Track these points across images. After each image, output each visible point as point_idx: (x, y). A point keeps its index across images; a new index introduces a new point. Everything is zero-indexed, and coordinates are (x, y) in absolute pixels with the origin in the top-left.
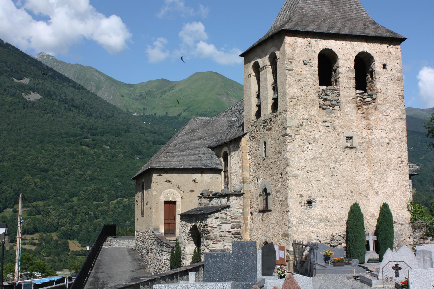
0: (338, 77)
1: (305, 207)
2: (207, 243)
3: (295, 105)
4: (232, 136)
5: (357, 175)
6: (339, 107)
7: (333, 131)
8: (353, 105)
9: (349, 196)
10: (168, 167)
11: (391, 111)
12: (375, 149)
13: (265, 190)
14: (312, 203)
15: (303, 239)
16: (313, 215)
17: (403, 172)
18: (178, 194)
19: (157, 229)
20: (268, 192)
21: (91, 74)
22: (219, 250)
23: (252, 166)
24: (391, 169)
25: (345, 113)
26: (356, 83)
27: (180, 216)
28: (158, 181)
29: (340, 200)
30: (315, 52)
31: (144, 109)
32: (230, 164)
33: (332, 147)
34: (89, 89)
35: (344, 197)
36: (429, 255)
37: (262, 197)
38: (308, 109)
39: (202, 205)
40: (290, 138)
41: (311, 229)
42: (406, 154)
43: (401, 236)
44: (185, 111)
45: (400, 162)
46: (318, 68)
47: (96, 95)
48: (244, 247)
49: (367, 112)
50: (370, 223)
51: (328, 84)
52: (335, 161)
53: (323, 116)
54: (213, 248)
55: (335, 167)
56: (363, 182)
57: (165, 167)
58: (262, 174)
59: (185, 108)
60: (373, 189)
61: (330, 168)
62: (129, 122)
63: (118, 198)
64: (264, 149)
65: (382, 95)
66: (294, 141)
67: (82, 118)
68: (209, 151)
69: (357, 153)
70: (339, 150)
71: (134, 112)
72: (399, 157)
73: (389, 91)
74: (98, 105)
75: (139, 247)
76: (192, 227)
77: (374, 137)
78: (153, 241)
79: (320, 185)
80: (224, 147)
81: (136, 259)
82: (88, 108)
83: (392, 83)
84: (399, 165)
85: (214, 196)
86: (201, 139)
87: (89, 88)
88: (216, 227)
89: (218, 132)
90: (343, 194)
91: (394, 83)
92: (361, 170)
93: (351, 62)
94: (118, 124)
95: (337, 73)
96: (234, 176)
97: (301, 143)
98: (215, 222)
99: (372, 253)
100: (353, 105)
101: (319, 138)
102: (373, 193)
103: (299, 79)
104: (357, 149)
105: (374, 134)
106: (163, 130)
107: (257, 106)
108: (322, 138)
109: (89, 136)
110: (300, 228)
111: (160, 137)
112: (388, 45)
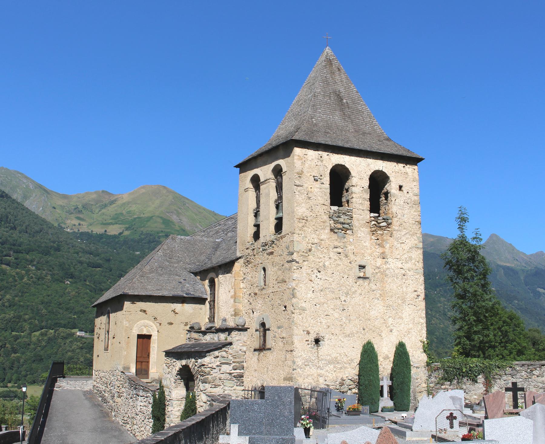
0: (350, 197)
1: (312, 346)
2: (204, 386)
3: (303, 226)
4: (219, 260)
5: (370, 310)
9: (361, 333)
10: (144, 294)
11: (407, 238)
12: (390, 280)
13: (263, 325)
14: (320, 341)
15: (310, 383)
16: (321, 355)
17: (419, 307)
18: (154, 327)
19: (128, 368)
20: (267, 327)
21: (18, 180)
22: (219, 396)
23: (247, 296)
24: (407, 304)
26: (370, 205)
27: (165, 353)
28: (131, 310)
29: (352, 338)
30: (327, 168)
33: (343, 277)
34: (15, 198)
35: (355, 335)
36: (459, 403)
37: (258, 332)
39: (192, 341)
43: (416, 381)
44: (127, 229)
46: (329, 186)
47: (22, 205)
48: (280, 393)
49: (382, 238)
50: (383, 366)
51: (340, 204)
53: (334, 241)
54: (210, 393)
57: (140, 294)
58: (259, 305)
59: (128, 226)
60: (388, 326)
61: (340, 301)
62: (61, 240)
63: (42, 329)
64: (262, 277)
65: (398, 220)
66: (301, 268)
67: (4, 231)
68: (191, 276)
69: (371, 284)
70: (351, 280)
71: (67, 227)
72: (415, 291)
73: (405, 216)
74: (24, 217)
75: (98, 390)
76: (181, 367)
77: (389, 266)
78: (122, 382)
79: (329, 320)
81: (95, 405)
82: (11, 220)
84: (415, 300)
85: (209, 331)
86: (181, 262)
87: (14, 197)
88: (215, 367)
89: (201, 254)
90: (354, 331)
91: (410, 207)
92: (374, 304)
93: (366, 181)
94: (48, 241)
95: (350, 192)
96: (223, 307)
98: (215, 361)
99: (386, 400)
100: (366, 230)
101: (330, 266)
102: (387, 331)
103: (309, 197)
104: (370, 280)
105: (388, 263)
106: (100, 250)
107: (255, 226)
108: (333, 266)
109: (12, 253)
110: (306, 371)
111: (96, 259)
112: (404, 165)
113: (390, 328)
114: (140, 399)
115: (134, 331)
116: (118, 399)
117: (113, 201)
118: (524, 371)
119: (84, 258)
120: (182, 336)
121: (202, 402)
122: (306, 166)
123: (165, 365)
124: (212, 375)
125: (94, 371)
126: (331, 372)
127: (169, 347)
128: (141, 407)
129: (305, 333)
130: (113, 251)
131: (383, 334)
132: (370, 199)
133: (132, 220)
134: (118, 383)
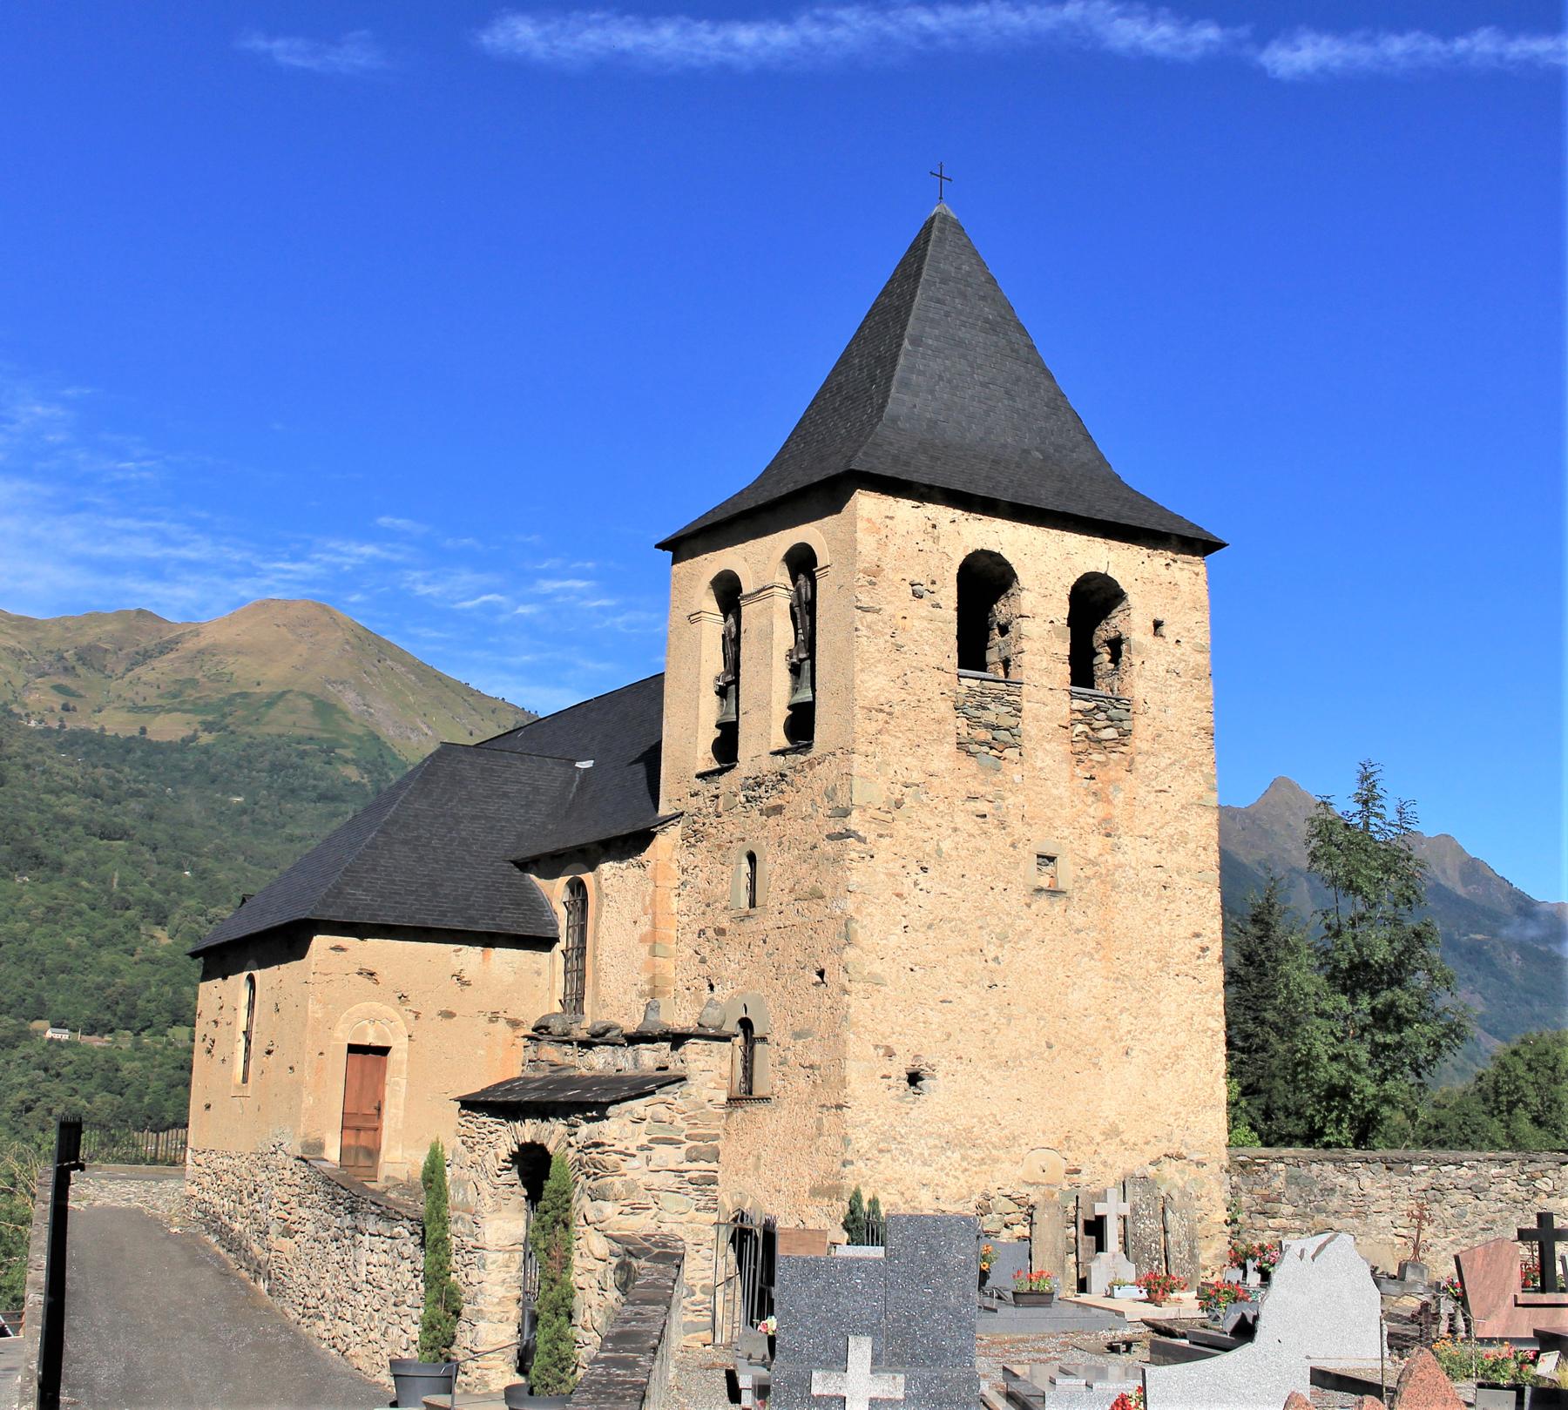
1: (901, 1092)
3: (880, 732)
6: (1018, 750)
7: (996, 831)
8: (1060, 748)
9: (1043, 1059)
11: (1174, 778)
12: (1124, 900)
14: (922, 1079)
16: (926, 1121)
17: (1207, 983)
18: (401, 1023)
20: (757, 1032)
22: (645, 1240)
24: (1172, 974)
25: (1036, 773)
30: (950, 559)
31: (66, 708)
32: (597, 926)
33: (992, 889)
35: (1025, 1062)
38: (921, 751)
40: (861, 846)
41: (918, 1169)
42: (1217, 924)
43: (1197, 1204)
44: (208, 727)
45: (1198, 952)
46: (956, 613)
48: (934, 1237)
50: (1104, 1156)
52: (1001, 937)
53: (968, 779)
54: (618, 1229)
55: (1000, 955)
56: (1085, 1013)
60: (1117, 1037)
66: (872, 857)
70: (1016, 898)
72: (1197, 935)
76: (516, 1149)
77: (1123, 860)
79: (949, 1016)
80: (571, 863)
83: (1179, 686)
88: (634, 1152)
91: (1184, 684)
92: (1079, 970)
97: (895, 867)
100: (1060, 748)
101: (954, 853)
103: (897, 645)
105: (1122, 851)
113: (1123, 1044)
114: (366, 1244)
115: (340, 1035)
116: (281, 1239)
117: (170, 642)
118: (1508, 1180)
119: (73, 807)
120: (482, 1052)
121: (591, 1258)
122: (891, 551)
123: (459, 1140)
124: (625, 1175)
125: (189, 1152)
126: (953, 1172)
127: (474, 1085)
128: (371, 1266)
129: (881, 1054)
130: (164, 791)
131: (1103, 1062)
132: (1070, 657)
133: (222, 699)
134: (282, 1193)
